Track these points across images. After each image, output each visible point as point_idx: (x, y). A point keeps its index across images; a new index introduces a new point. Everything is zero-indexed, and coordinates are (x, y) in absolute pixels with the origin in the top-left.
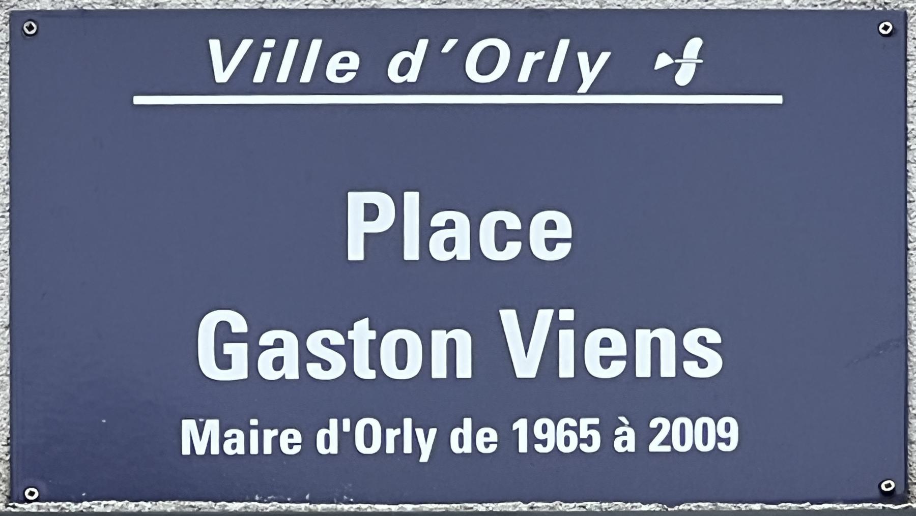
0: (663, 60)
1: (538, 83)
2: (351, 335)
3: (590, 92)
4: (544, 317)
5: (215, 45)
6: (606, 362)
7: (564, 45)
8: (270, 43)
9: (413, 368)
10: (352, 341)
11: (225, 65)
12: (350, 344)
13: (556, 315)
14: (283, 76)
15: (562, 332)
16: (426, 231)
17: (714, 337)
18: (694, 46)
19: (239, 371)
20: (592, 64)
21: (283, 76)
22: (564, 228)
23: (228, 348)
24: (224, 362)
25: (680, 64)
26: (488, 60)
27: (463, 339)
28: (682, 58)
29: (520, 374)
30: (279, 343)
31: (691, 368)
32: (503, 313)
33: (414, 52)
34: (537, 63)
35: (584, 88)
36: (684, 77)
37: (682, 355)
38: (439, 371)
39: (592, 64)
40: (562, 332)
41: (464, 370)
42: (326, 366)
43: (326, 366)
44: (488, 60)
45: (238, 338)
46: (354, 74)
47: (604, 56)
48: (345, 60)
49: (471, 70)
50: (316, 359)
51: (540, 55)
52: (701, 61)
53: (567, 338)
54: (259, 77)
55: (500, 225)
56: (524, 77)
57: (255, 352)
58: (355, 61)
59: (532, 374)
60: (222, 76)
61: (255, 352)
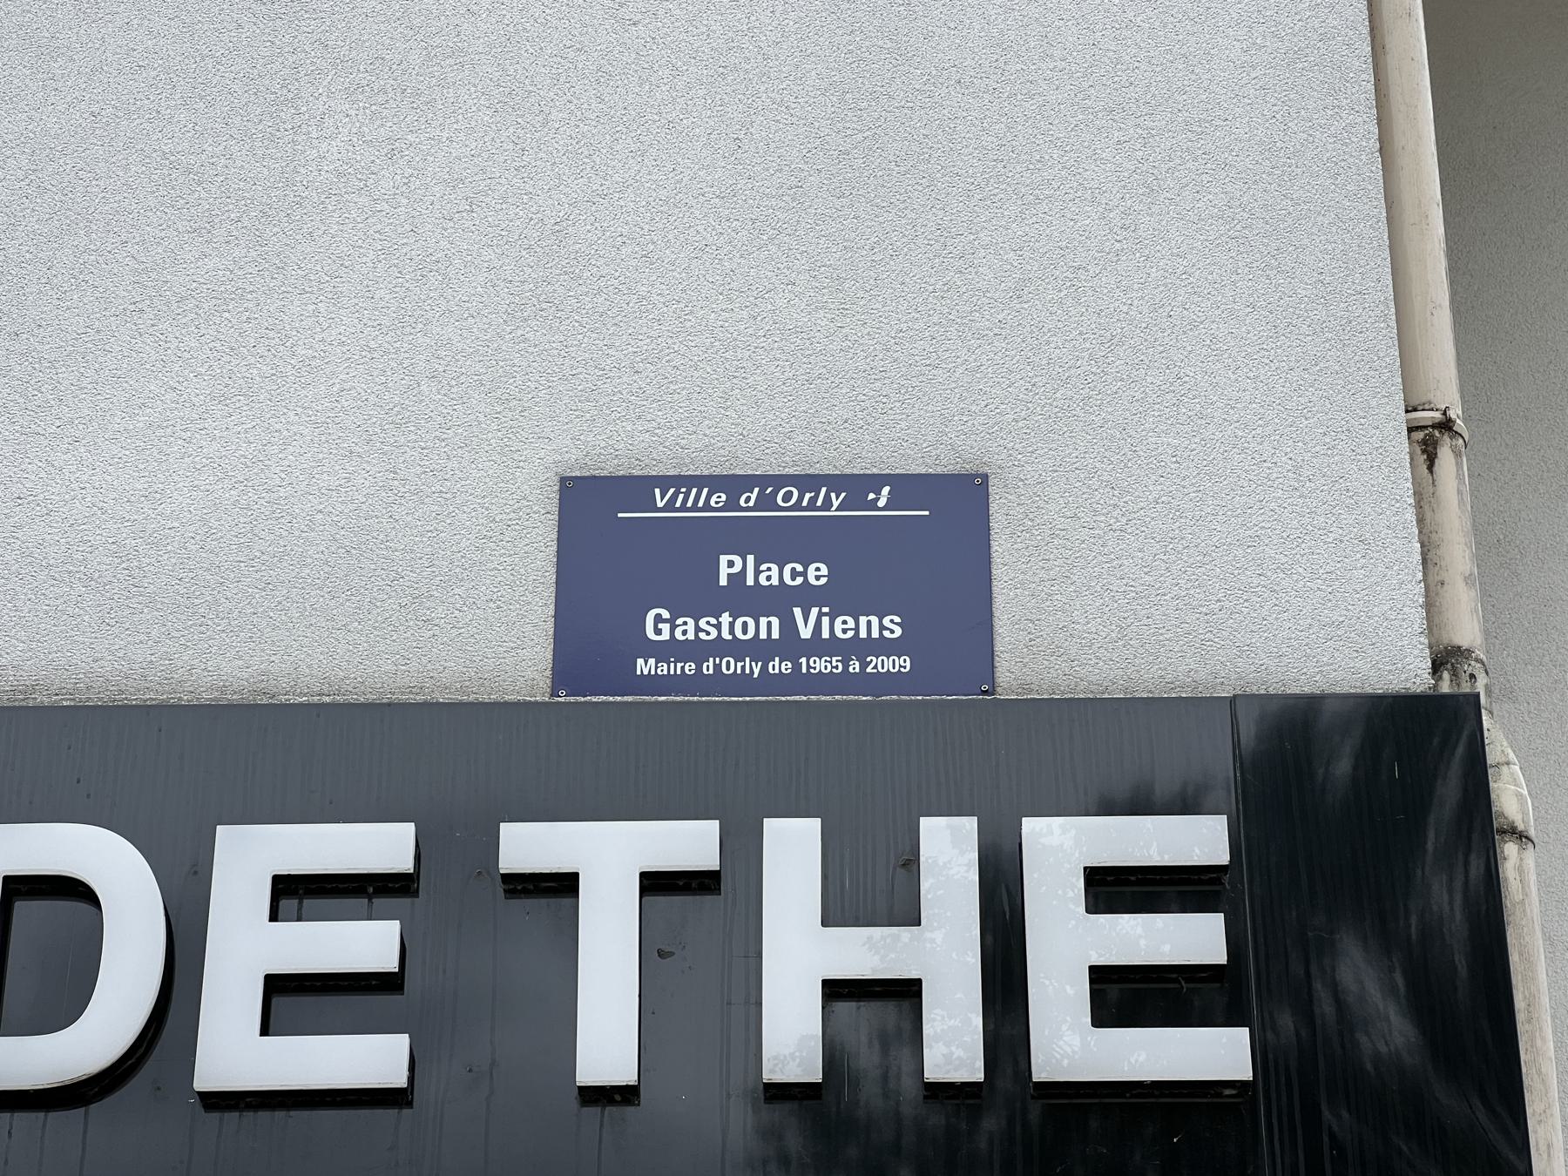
0: (872, 496)
1: (812, 505)
2: (720, 619)
5: (657, 491)
6: (845, 631)
7: (824, 490)
8: (683, 490)
13: (820, 610)
14: (689, 504)
15: (823, 618)
16: (757, 573)
17: (897, 619)
18: (886, 490)
19: (665, 636)
21: (689, 504)
22: (824, 570)
23: (660, 626)
24: (658, 632)
27: (775, 621)
31: (887, 634)
34: (742, 666)
35: (833, 509)
36: (881, 503)
37: (882, 628)
40: (823, 618)
41: (775, 635)
42: (708, 633)
43: (708, 633)
45: (665, 621)
47: (843, 495)
48: (719, 497)
51: (813, 494)
53: (826, 620)
54: (678, 505)
55: (793, 569)
56: (805, 503)
58: (724, 497)
59: (809, 637)
60: (660, 504)
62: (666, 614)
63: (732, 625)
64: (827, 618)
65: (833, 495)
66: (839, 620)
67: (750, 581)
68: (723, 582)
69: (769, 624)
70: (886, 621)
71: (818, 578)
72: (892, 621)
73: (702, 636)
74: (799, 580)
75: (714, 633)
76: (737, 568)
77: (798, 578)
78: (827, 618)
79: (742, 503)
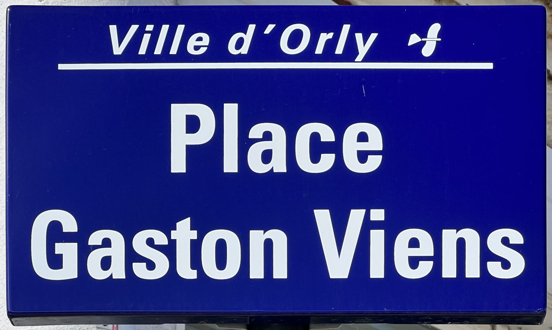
0: (414, 39)
2: (174, 235)
3: (365, 60)
5: (113, 29)
6: (414, 262)
7: (346, 28)
8: (150, 28)
10: (175, 240)
11: (120, 42)
12: (172, 244)
14: (158, 50)
17: (516, 237)
18: (435, 29)
20: (365, 40)
21: (158, 50)
23: (60, 248)
28: (426, 37)
29: (333, 275)
30: (107, 243)
33: (245, 33)
34: (328, 42)
35: (360, 58)
36: (428, 50)
39: (365, 40)
42: (151, 266)
43: (151, 266)
45: (68, 238)
47: (373, 36)
48: (200, 39)
50: (141, 259)
51: (331, 35)
52: (440, 40)
54: (143, 51)
55: (315, 137)
56: (319, 50)
58: (206, 39)
59: (344, 275)
60: (118, 50)
65: (359, 36)
71: (363, 156)
79: (232, 49)
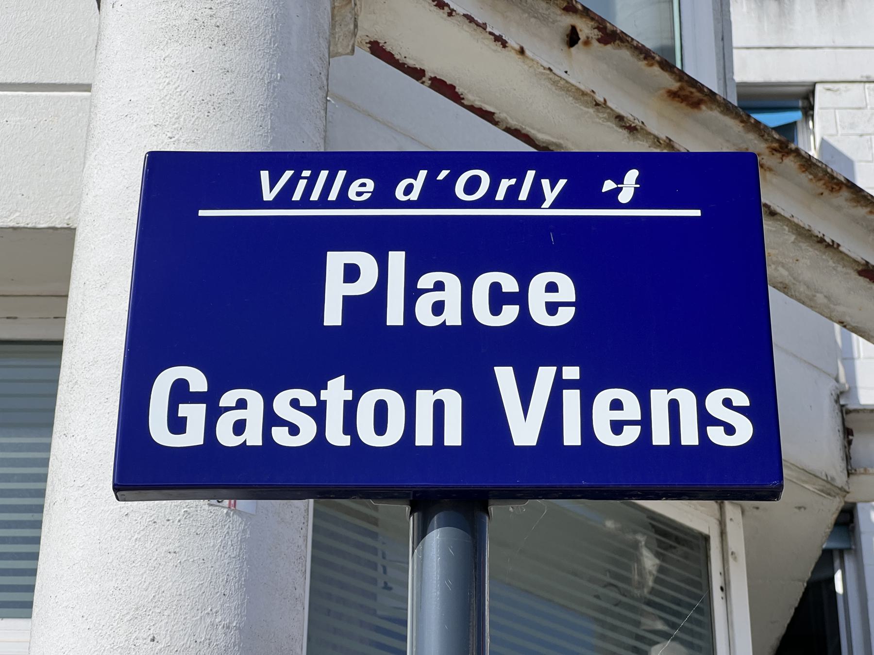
0: (609, 185)
1: (511, 199)
2: (324, 396)
3: (551, 207)
4: (545, 376)
5: (265, 175)
6: (617, 427)
7: (531, 175)
8: (306, 173)
9: (394, 434)
11: (272, 187)
13: (559, 373)
14: (315, 196)
15: (566, 392)
16: (412, 294)
17: (741, 398)
19: (194, 436)
20: (552, 188)
21: (315, 196)
22: (567, 289)
23: (184, 410)
24: (177, 425)
25: (621, 189)
26: (472, 185)
27: (452, 400)
31: (716, 435)
32: (310, 172)
33: (416, 179)
34: (510, 188)
35: (547, 204)
36: (625, 196)
37: (705, 419)
38: (424, 437)
39: (552, 188)
40: (566, 392)
41: (453, 437)
42: (294, 430)
43: (294, 430)
44: (472, 185)
45: (196, 398)
46: (370, 194)
47: (562, 183)
48: (363, 185)
49: (459, 190)
51: (513, 181)
52: (638, 186)
53: (572, 399)
54: (297, 196)
55: (495, 288)
56: (500, 196)
57: (214, 414)
58: (370, 185)
60: (268, 196)
61: (214, 414)
62: (198, 381)
63: (350, 410)
64: (577, 393)
65: (545, 183)
66: (603, 399)
67: (395, 316)
68: (333, 316)
69: (439, 407)
70: (714, 401)
71: (552, 308)
72: (727, 403)
73: (281, 436)
74: (510, 314)
75: (308, 431)
76: (365, 285)
77: (505, 308)
78: (577, 393)
